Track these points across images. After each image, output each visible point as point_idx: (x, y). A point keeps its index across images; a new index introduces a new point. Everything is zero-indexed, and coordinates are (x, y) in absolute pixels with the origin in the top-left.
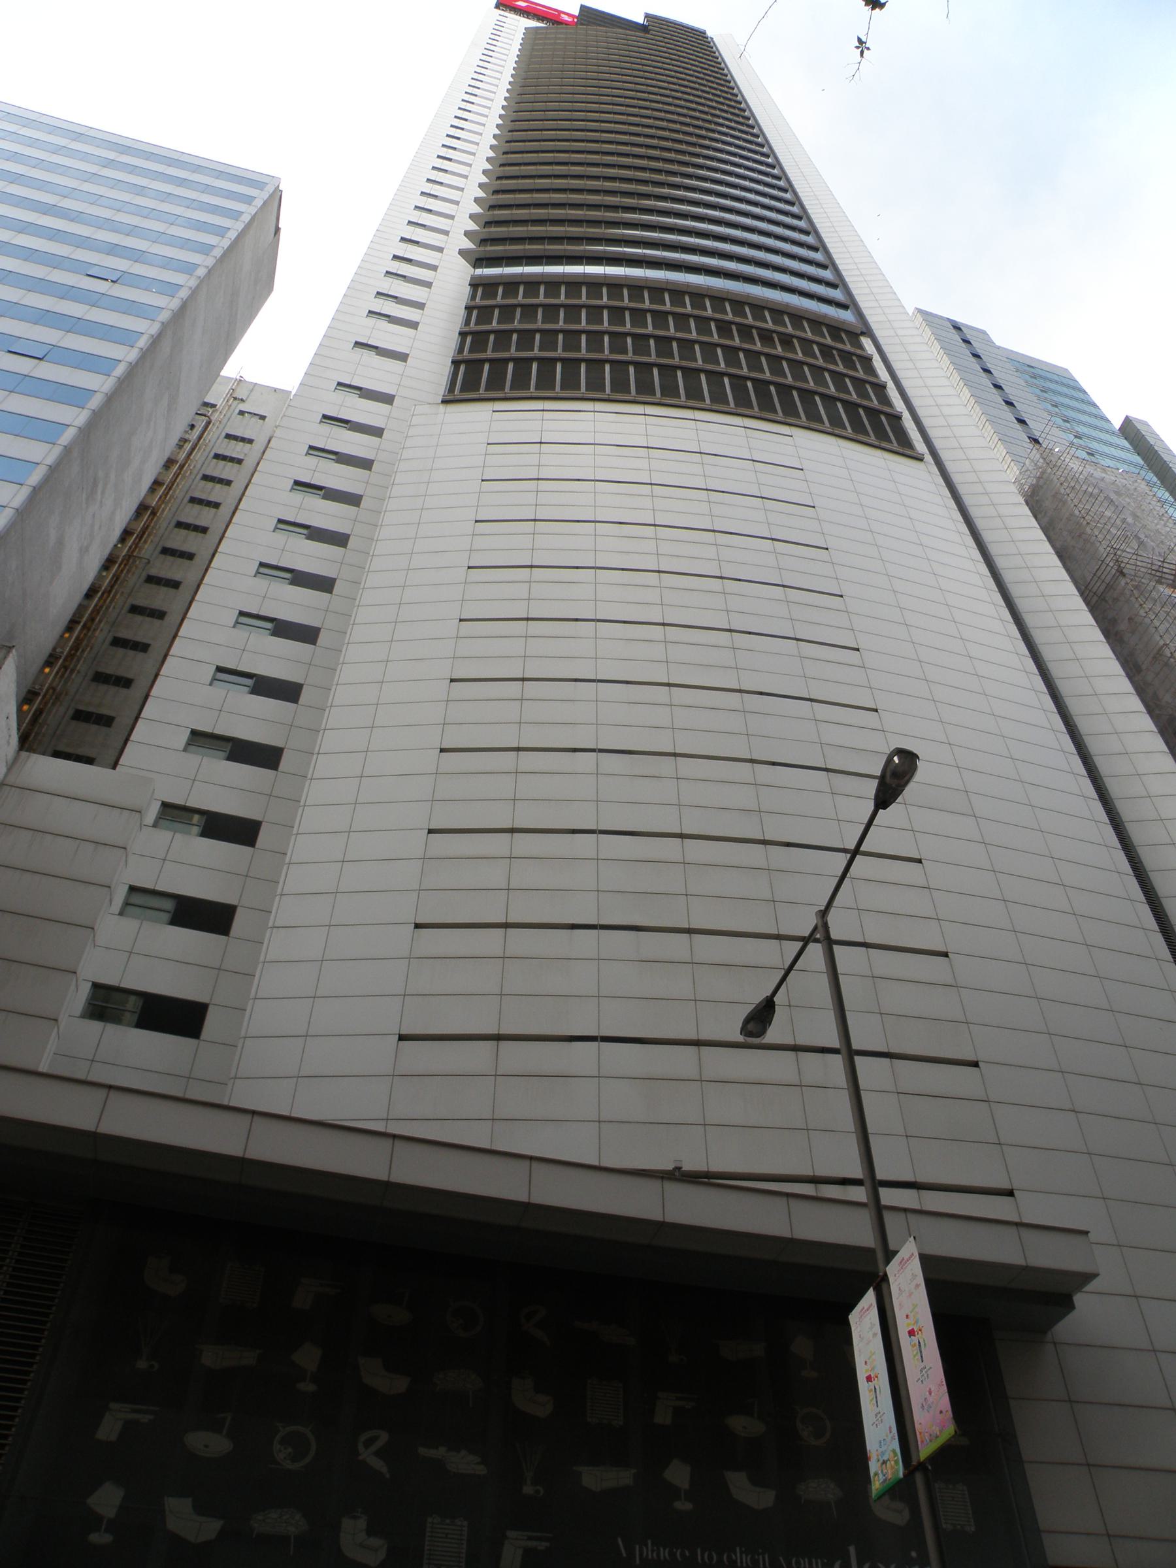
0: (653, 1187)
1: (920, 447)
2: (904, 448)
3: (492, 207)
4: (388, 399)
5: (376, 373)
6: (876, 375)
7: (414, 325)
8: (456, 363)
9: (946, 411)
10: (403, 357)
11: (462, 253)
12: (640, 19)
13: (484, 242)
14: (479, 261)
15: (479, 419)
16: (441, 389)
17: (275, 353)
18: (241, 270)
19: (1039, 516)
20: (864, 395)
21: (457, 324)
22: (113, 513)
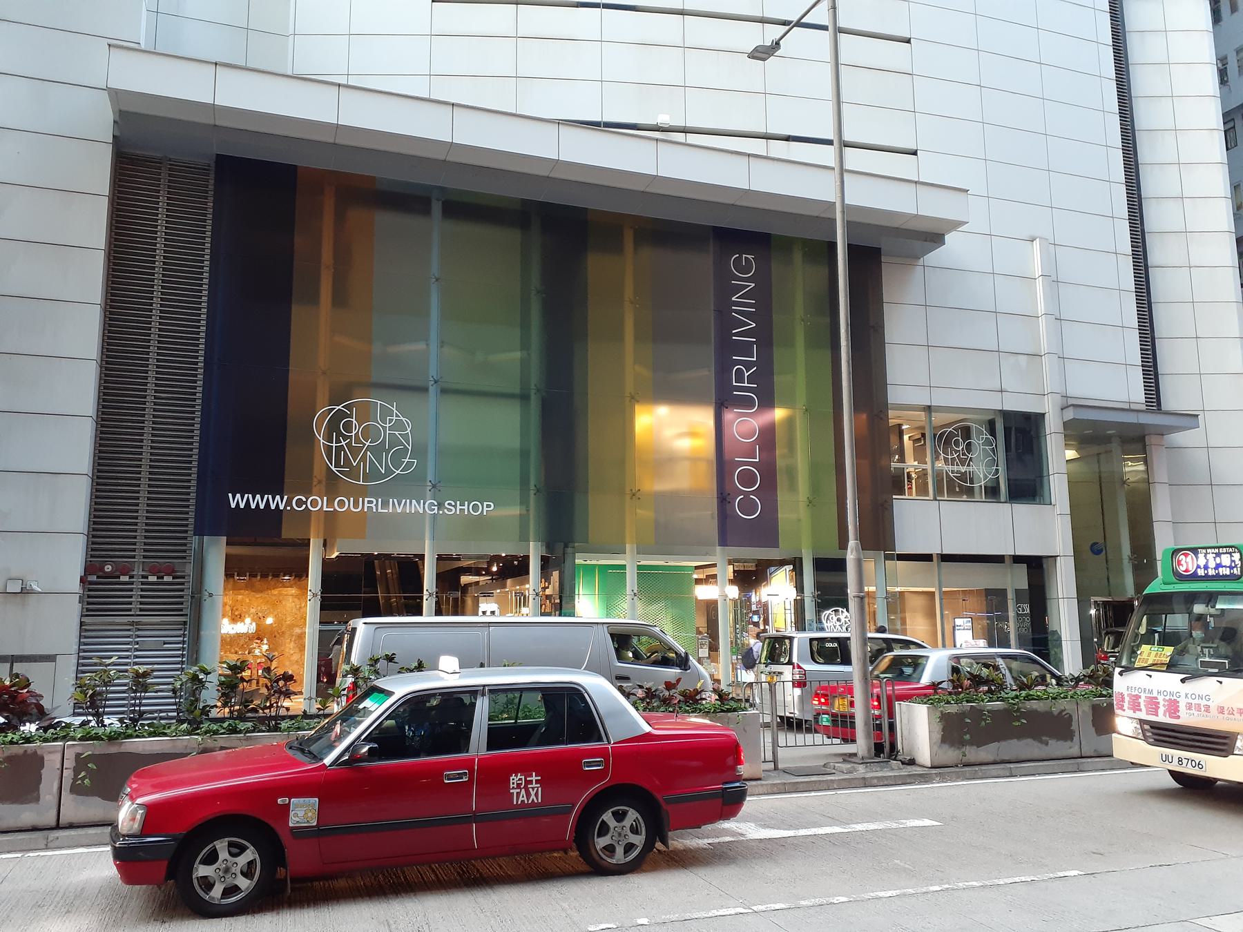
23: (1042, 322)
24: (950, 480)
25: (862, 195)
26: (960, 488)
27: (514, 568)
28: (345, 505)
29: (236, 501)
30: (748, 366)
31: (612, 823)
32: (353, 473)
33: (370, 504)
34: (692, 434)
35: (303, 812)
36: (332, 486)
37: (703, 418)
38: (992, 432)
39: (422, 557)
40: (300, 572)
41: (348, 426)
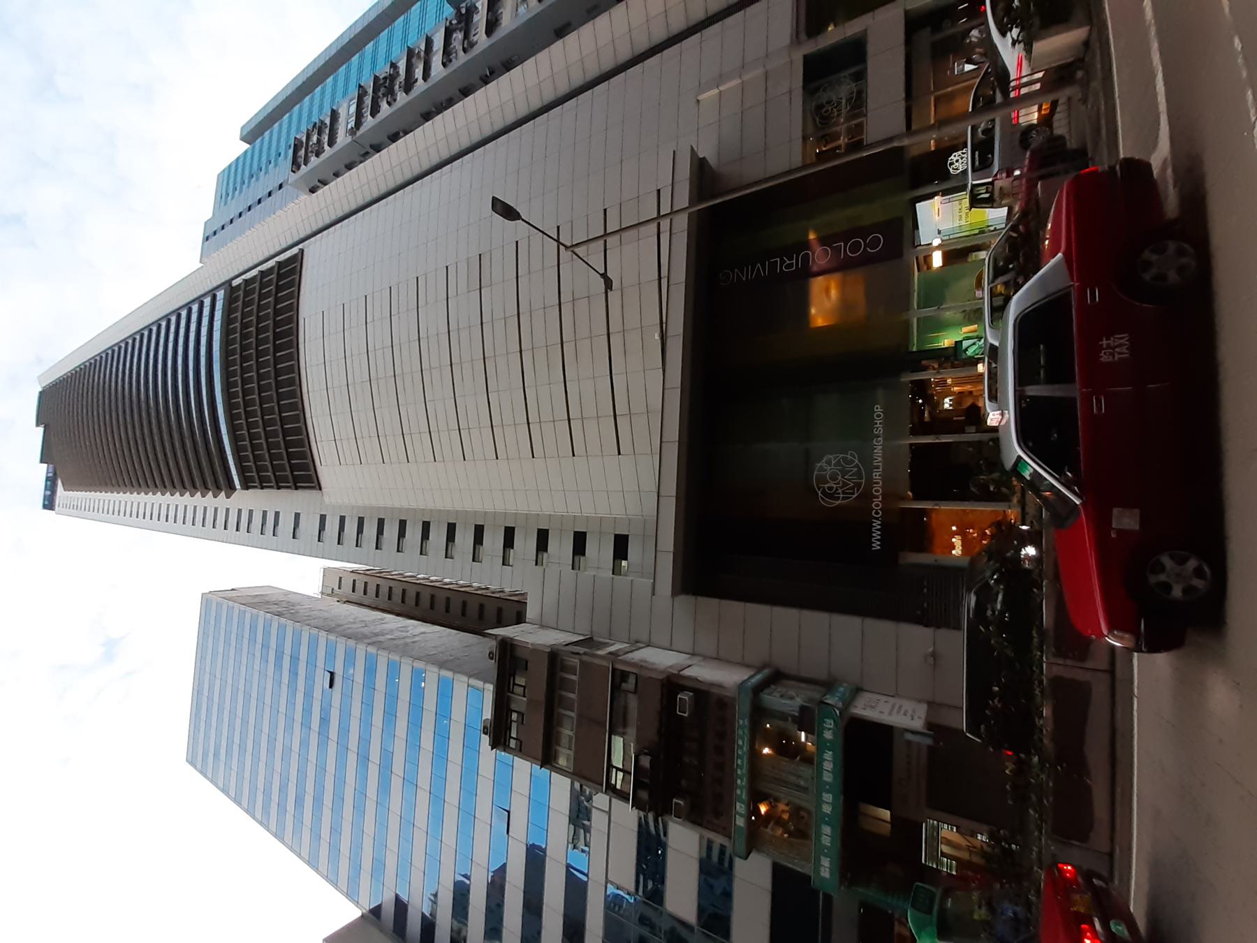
0: (669, 343)
1: (295, 250)
2: (298, 260)
3: (195, 487)
4: (323, 519)
5: (310, 525)
6: (272, 268)
7: (277, 514)
8: (297, 488)
9: (323, 205)
10: (297, 516)
11: (228, 497)
12: (41, 429)
13: (195, 487)
14: (231, 488)
15: (325, 473)
16: (314, 493)
17: (301, 574)
18: (277, 606)
19: (205, 260)
20: (269, 283)
21: (274, 492)
22: (393, 623)
23: (746, 77)
24: (852, 109)
25: (683, 200)
26: (858, 103)
27: (921, 388)
28: (878, 489)
29: (876, 546)
30: (783, 262)
31: (1154, 271)
32: (858, 485)
33: (877, 476)
34: (827, 290)
35: (1126, 520)
36: (867, 496)
37: (817, 284)
38: (817, 89)
39: (911, 445)
40: (923, 512)
41: (830, 488)
